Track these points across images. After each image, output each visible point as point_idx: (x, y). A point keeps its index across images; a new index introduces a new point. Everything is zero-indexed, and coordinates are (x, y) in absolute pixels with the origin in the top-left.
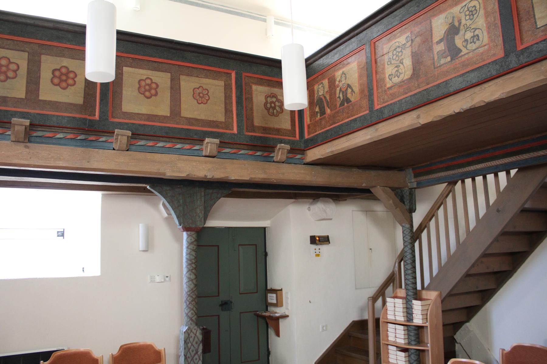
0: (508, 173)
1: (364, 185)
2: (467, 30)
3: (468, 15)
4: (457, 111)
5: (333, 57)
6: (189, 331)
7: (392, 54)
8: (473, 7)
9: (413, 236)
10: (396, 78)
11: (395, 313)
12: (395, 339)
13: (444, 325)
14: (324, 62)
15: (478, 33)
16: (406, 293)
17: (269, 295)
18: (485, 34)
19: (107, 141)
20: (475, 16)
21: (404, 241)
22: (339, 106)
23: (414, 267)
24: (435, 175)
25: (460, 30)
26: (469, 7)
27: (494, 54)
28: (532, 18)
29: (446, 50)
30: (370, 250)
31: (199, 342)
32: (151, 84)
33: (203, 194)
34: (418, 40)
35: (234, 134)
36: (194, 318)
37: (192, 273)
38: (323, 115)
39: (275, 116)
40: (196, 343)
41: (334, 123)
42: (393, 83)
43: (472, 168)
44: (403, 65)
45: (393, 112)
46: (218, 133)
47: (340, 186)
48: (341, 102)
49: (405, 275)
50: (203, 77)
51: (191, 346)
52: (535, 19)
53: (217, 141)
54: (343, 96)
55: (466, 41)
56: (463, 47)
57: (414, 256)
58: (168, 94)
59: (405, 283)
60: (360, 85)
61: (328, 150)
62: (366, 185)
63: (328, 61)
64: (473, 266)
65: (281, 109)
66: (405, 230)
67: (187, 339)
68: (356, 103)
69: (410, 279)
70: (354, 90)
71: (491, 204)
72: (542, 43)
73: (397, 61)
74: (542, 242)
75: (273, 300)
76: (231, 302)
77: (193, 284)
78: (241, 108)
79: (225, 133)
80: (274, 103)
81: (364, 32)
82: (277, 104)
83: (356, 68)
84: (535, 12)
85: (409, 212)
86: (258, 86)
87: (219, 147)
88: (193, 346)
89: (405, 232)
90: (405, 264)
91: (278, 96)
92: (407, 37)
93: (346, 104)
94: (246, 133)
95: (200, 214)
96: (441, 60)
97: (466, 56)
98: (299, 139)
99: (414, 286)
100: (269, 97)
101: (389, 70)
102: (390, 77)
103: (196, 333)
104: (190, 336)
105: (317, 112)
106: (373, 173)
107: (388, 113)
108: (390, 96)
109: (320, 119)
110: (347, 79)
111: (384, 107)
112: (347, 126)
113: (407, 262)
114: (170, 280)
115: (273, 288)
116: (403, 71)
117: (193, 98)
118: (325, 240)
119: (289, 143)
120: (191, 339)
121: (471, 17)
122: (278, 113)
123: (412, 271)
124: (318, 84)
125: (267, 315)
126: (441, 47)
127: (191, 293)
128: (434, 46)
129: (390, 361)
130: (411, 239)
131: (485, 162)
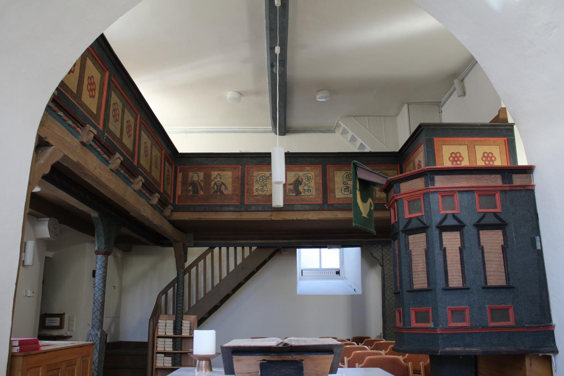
0: (251, 248)
4: (294, 219)
10: (261, 192)
18: (314, 191)
27: (317, 201)
55: (304, 189)
73: (263, 183)
97: (304, 197)
105: (190, 191)
116: (266, 190)
121: (308, 180)
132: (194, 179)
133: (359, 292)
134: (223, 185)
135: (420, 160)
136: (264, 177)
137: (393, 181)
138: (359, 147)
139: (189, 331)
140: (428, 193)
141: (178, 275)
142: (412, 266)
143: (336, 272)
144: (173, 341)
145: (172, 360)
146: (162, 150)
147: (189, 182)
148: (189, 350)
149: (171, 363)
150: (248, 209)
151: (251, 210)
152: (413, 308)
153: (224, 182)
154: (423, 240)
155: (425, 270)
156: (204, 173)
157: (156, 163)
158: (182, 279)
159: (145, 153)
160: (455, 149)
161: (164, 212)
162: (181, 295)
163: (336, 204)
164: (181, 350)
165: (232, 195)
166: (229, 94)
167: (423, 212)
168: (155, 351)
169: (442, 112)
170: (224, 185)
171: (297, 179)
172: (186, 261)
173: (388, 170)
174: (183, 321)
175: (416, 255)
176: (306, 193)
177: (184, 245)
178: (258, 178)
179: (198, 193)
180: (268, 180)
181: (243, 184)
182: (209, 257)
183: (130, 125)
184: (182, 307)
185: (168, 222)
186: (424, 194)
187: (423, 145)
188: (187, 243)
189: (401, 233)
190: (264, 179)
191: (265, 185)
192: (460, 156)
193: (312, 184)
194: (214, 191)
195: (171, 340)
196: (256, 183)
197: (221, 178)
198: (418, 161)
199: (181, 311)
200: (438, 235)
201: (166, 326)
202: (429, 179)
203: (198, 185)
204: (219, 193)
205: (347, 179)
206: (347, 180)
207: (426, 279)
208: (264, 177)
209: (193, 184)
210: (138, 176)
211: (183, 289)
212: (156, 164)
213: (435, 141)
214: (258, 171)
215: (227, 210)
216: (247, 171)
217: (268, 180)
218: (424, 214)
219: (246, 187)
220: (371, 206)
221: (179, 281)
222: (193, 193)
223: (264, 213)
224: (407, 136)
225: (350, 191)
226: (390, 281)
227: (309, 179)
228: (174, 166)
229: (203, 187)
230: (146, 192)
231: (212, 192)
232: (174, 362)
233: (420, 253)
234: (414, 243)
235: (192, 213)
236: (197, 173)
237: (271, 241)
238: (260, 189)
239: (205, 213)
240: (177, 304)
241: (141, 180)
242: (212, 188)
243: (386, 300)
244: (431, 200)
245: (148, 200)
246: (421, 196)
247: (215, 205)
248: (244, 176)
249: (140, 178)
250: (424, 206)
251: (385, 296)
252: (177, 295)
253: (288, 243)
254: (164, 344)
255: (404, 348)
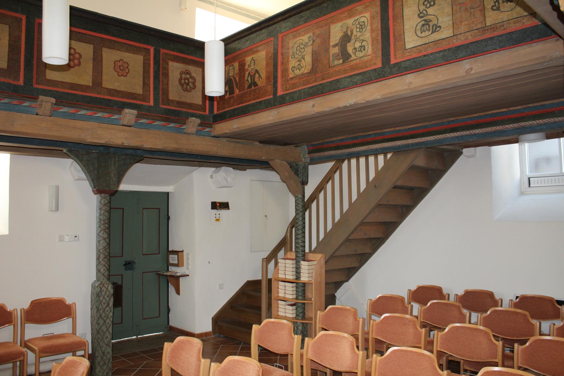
0: (385, 157)
1: (264, 158)
2: (357, 40)
3: (358, 28)
5: (244, 44)
6: (101, 286)
7: (296, 49)
8: (362, 22)
9: (304, 205)
10: (298, 70)
11: (285, 273)
12: (284, 295)
13: (327, 283)
14: (236, 47)
15: (364, 44)
16: (296, 255)
17: (171, 256)
18: (370, 46)
19: (30, 106)
20: (363, 29)
21: (297, 210)
22: (246, 88)
23: (304, 233)
24: (326, 153)
25: (351, 39)
26: (360, 21)
28: (402, 40)
29: (339, 54)
30: (266, 217)
31: (110, 296)
32: (74, 54)
33: (117, 159)
34: (318, 41)
35: (151, 106)
36: (106, 274)
37: (104, 232)
38: (232, 95)
39: (188, 92)
40: (108, 296)
41: (242, 103)
42: (295, 74)
43: (357, 149)
44: (305, 60)
45: (293, 99)
46: (136, 105)
47: (243, 157)
48: (249, 84)
49: (295, 239)
50: (124, 51)
51: (103, 299)
52: (405, 42)
53: (135, 112)
54: (251, 80)
55: (355, 49)
56: (352, 53)
57: (304, 223)
58: (90, 65)
59: (295, 246)
60: (267, 72)
61: (235, 126)
62: (265, 158)
63: (239, 46)
64: (353, 232)
65: (193, 85)
66: (297, 200)
67: (99, 293)
68: (262, 87)
70: (261, 76)
71: (370, 181)
72: (408, 61)
73: (300, 56)
74: (410, 214)
75: (175, 261)
76: (135, 263)
77: (105, 243)
78: (158, 82)
79: (142, 105)
80: (188, 80)
81: (274, 26)
82: (191, 80)
83: (265, 56)
84: (405, 36)
85: (302, 184)
86: (174, 63)
87: (136, 117)
88: (105, 299)
89: (297, 201)
90: (296, 229)
91: (192, 73)
92: (309, 37)
93: (253, 87)
94: (162, 106)
95: (114, 178)
96: (335, 61)
97: (355, 61)
98: (209, 114)
99: (303, 249)
100: (183, 73)
101: (293, 63)
102: (293, 69)
103: (108, 287)
104: (102, 290)
106: (272, 147)
107: (289, 99)
108: (292, 86)
109: (230, 98)
110: (256, 65)
111: (287, 94)
112: (253, 107)
113: (298, 227)
114: (78, 240)
115: (174, 250)
117: (114, 70)
118: (225, 206)
119: (200, 117)
120: (103, 293)
121: (361, 30)
122: (191, 89)
123: (302, 236)
124: (229, 65)
125: (168, 274)
126: (336, 50)
127: (104, 250)
128: (330, 48)
129: (279, 314)
130: (302, 207)
131: (368, 145)
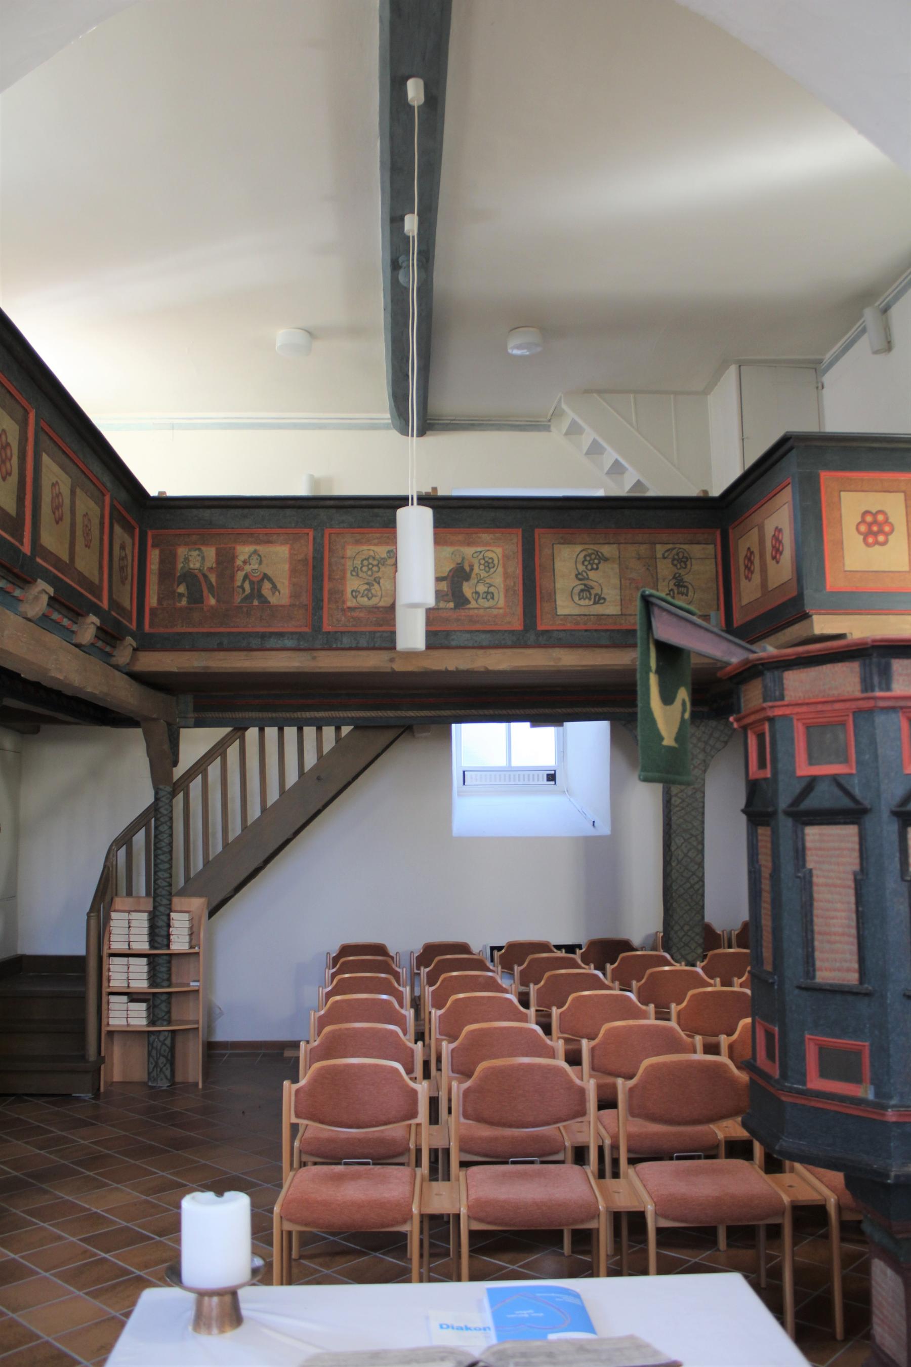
0: (338, 729)
4: (450, 668)
10: (366, 599)
27: (509, 623)
44: (380, 586)
55: (477, 593)
69: (167, 878)
97: (476, 611)
105: (181, 595)
116: (379, 594)
121: (487, 569)
132: (192, 566)
133: (604, 829)
134: (266, 581)
135: (779, 527)
136: (374, 558)
137: (762, 664)
138: (610, 468)
139: (187, 939)
140: (871, 711)
141: (157, 799)
142: (812, 915)
143: (548, 775)
144: (149, 964)
145: (148, 1009)
146: (104, 495)
147: (179, 574)
148: (188, 985)
149: (146, 971)
150: (331, 642)
151: (339, 646)
152: (812, 1035)
153: (270, 573)
154: (849, 845)
155: (854, 931)
156: (217, 549)
157: (87, 533)
158: (167, 810)
159: (54, 513)
160: (873, 501)
161: (114, 656)
162: (164, 849)
163: (557, 630)
164: (169, 986)
165: (290, 606)
166: (282, 335)
167: (854, 764)
168: (105, 990)
169: (823, 387)
170: (269, 579)
171: (458, 564)
172: (175, 763)
173: (691, 543)
174: (173, 915)
175: (827, 885)
176: (481, 601)
177: (169, 724)
178: (358, 563)
179: (203, 603)
180: (383, 569)
181: (317, 578)
182: (233, 752)
183: (8, 445)
184: (168, 880)
185: (125, 677)
186: (857, 713)
187: (789, 488)
188: (178, 719)
189: (781, 817)
190: (373, 566)
191: (375, 580)
192: (886, 521)
193: (498, 579)
194: (243, 595)
195: (144, 961)
196: (352, 575)
197: (260, 563)
198: (775, 527)
199: (167, 888)
200: (895, 837)
201: (129, 927)
202: (875, 670)
203: (202, 579)
204: (256, 603)
205: (586, 566)
206: (586, 568)
207: (855, 957)
208: (374, 558)
209: (190, 578)
210: (36, 581)
211: (171, 835)
212: (87, 534)
213: (822, 481)
214: (358, 542)
215: (278, 646)
216: (330, 543)
217: (383, 569)
218: (854, 771)
219: (327, 586)
220: (684, 711)
221: (159, 816)
222: (189, 602)
223: (372, 653)
224: (735, 472)
225: (595, 597)
226: (683, 811)
227: (488, 565)
228: (137, 531)
229: (214, 584)
230: (60, 616)
231: (239, 600)
232: (154, 1015)
233: (839, 882)
234: (820, 849)
235: (188, 655)
236: (200, 550)
237: (391, 714)
238: (362, 592)
239: (222, 654)
240: (155, 873)
241: (44, 591)
242: (238, 589)
243: (674, 858)
244: (877, 731)
245: (67, 634)
246: (848, 715)
247: (247, 633)
248: (322, 559)
249: (41, 585)
250: (856, 746)
251: (670, 850)
252: (155, 850)
253: (431, 717)
254: (129, 934)
255: (784, 1144)
